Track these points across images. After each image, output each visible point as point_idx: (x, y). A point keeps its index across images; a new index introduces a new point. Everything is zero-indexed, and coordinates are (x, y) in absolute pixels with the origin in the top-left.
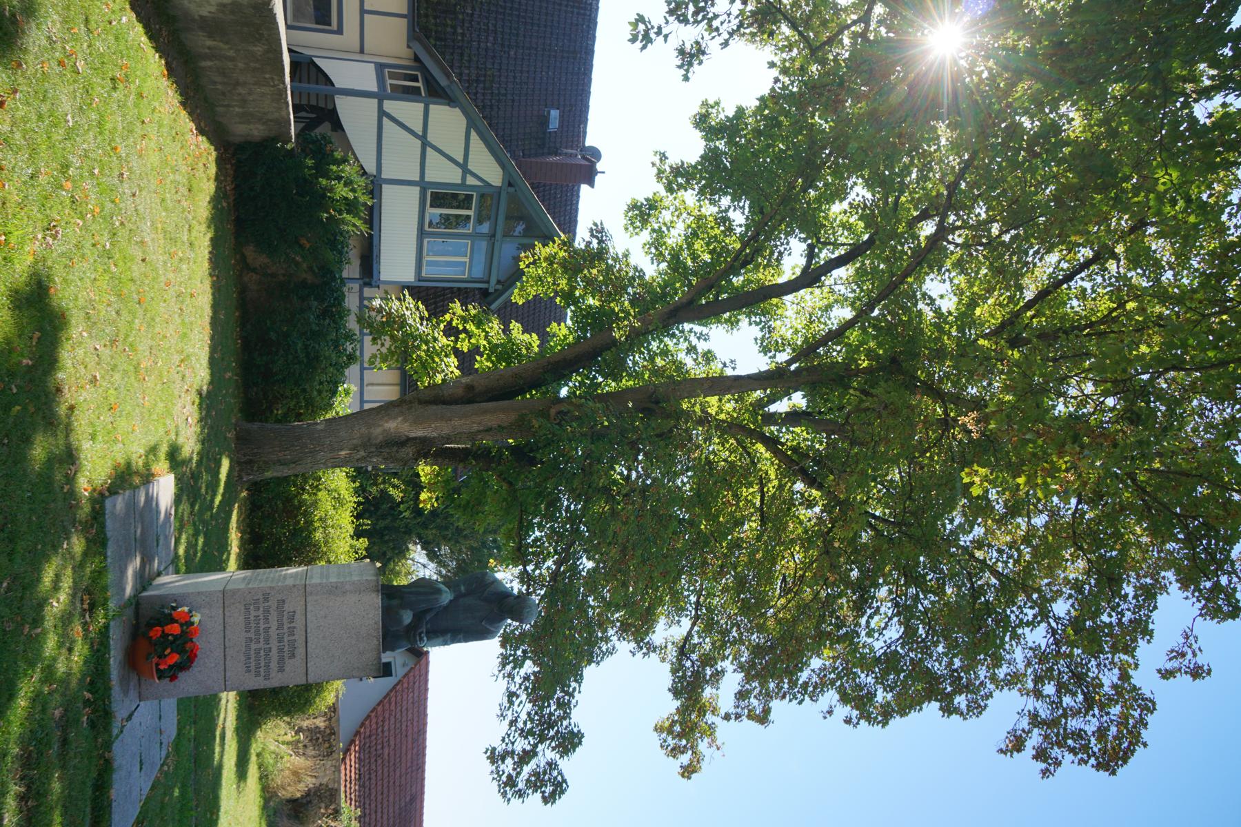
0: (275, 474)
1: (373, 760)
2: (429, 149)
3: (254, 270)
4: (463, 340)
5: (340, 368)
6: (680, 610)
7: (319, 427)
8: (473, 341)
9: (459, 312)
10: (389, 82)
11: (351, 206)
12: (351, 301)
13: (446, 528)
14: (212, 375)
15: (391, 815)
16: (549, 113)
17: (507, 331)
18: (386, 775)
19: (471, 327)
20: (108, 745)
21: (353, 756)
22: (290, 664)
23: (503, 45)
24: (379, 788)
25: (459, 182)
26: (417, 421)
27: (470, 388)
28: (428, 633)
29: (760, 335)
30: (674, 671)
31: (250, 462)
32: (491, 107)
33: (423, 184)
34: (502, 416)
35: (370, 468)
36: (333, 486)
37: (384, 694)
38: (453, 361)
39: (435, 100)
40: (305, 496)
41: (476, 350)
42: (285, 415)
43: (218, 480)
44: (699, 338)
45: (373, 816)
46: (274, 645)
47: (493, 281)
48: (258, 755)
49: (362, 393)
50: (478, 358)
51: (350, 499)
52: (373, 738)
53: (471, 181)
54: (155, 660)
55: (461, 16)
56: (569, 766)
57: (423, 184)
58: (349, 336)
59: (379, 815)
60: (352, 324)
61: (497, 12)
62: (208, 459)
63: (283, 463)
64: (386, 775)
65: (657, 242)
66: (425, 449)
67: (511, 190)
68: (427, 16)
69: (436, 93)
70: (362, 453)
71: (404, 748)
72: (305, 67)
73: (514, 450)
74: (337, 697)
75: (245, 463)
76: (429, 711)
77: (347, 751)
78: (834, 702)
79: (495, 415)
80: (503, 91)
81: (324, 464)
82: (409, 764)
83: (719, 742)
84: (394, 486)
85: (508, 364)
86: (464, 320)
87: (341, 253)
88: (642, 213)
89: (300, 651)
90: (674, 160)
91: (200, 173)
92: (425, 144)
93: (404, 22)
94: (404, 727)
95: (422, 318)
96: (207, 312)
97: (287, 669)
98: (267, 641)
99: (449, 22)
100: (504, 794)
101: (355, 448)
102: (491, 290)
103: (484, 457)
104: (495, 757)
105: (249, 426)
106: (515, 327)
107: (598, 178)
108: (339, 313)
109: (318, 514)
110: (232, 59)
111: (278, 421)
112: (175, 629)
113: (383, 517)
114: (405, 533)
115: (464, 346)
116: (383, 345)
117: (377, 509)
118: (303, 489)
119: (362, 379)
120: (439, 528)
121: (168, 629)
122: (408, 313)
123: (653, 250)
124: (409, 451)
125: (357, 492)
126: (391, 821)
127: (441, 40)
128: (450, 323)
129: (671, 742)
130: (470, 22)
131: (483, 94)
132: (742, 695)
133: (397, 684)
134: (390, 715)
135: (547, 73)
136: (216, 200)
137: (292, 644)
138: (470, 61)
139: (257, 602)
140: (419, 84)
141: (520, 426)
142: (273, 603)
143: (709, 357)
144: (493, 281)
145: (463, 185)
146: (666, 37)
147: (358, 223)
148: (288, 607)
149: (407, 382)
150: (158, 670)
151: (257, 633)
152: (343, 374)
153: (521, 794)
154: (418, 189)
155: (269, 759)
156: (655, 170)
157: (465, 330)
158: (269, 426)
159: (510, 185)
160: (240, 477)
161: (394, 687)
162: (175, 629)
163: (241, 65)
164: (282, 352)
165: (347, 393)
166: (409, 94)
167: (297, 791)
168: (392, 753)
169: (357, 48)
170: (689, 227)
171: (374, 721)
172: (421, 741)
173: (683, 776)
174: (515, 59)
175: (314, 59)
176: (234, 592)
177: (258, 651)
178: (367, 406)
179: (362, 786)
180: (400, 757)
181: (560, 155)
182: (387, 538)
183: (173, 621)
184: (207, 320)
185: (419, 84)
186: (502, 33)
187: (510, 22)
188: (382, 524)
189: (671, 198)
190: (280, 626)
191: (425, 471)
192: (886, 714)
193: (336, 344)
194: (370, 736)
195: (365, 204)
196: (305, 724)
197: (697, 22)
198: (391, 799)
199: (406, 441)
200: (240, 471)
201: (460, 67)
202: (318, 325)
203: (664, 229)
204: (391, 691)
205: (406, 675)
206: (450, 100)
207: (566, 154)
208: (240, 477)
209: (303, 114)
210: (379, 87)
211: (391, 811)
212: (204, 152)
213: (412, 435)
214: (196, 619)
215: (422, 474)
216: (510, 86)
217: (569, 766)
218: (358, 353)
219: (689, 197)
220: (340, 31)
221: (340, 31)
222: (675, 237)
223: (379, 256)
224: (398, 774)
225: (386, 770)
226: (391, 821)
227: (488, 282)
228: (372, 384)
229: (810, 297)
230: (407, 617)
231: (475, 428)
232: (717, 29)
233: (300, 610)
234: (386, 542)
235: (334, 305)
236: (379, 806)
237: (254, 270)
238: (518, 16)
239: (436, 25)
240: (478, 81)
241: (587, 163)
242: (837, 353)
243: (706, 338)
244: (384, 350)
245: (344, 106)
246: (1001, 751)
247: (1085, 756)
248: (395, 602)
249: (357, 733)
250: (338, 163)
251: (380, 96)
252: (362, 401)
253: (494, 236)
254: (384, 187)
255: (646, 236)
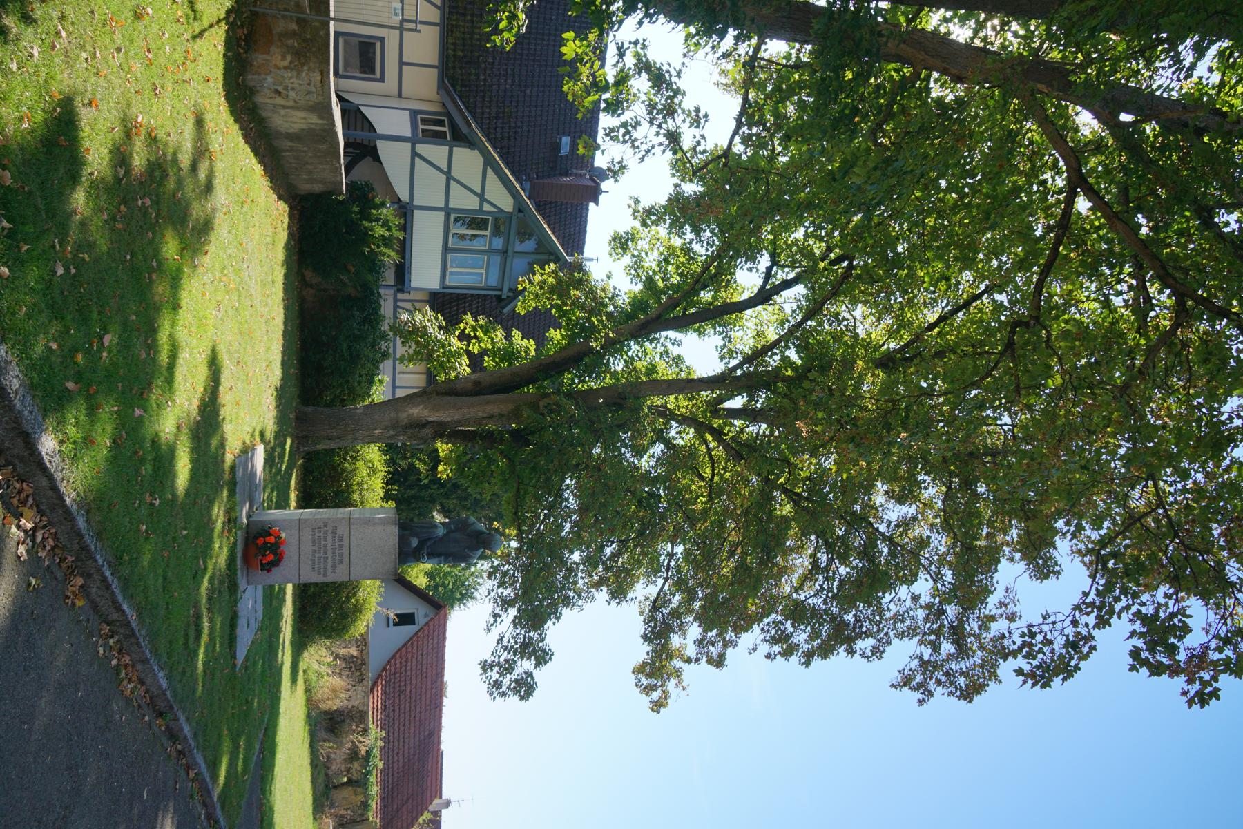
0: (325, 447)
1: (397, 695)
2: (452, 182)
3: (311, 286)
4: (474, 344)
5: (376, 364)
6: (656, 571)
7: (358, 411)
8: (482, 345)
9: (471, 322)
10: (421, 127)
11: (387, 241)
12: (386, 308)
13: (466, 499)
14: (283, 373)
15: (412, 745)
16: (561, 139)
17: (508, 337)
18: (408, 709)
19: (480, 334)
20: (236, 602)
21: (379, 690)
22: (340, 568)
23: (520, 86)
24: (402, 720)
25: (478, 208)
26: (435, 409)
27: (477, 383)
28: (428, 555)
29: (721, 343)
30: (647, 622)
31: (306, 437)
32: (509, 139)
33: (447, 211)
34: (501, 406)
35: (400, 444)
36: (368, 458)
37: (408, 638)
38: (465, 360)
39: (459, 143)
40: (346, 465)
41: (484, 352)
42: (333, 400)
43: (285, 450)
44: (673, 344)
45: (396, 743)
46: (330, 555)
47: (506, 289)
48: (305, 672)
49: (394, 380)
50: (486, 358)
51: (382, 470)
52: (397, 675)
53: (487, 207)
54: (260, 557)
55: (483, 66)
56: (541, 675)
57: (447, 211)
58: (384, 337)
59: (401, 744)
60: (385, 327)
61: (515, 59)
62: (280, 436)
63: (330, 438)
64: (408, 709)
65: (637, 266)
66: (442, 431)
67: (521, 215)
68: (454, 68)
69: (460, 138)
70: (392, 432)
71: (424, 688)
72: (353, 115)
73: (513, 433)
74: (367, 626)
75: (303, 437)
76: (447, 657)
77: (375, 684)
78: (758, 641)
79: (497, 405)
80: (519, 124)
81: (362, 440)
82: (428, 702)
83: (684, 684)
84: (420, 460)
85: (510, 364)
86: (474, 329)
87: (378, 273)
88: (621, 243)
89: (346, 560)
90: (646, 203)
91: (280, 229)
92: (449, 178)
93: (435, 71)
94: (424, 670)
95: (440, 328)
96: (281, 327)
97: (338, 571)
98: (325, 553)
99: (473, 71)
100: (491, 695)
101: (386, 428)
102: (504, 297)
103: (490, 438)
104: (486, 667)
105: (306, 409)
106: (516, 333)
107: (602, 197)
108: (376, 320)
109: (356, 480)
110: (305, 152)
111: (327, 405)
112: (272, 539)
113: (410, 487)
114: (430, 502)
115: (475, 349)
116: (410, 347)
117: (406, 480)
118: (345, 459)
119: (394, 368)
120: (461, 499)
121: (267, 539)
122: (428, 324)
123: (633, 272)
124: (428, 432)
125: (387, 463)
126: (412, 750)
127: (466, 86)
128: (463, 331)
129: (644, 681)
130: (492, 69)
131: (502, 128)
132: (700, 643)
133: (419, 631)
134: (412, 657)
135: (560, 105)
136: (288, 247)
137: (341, 555)
138: (490, 102)
139: (320, 528)
140: (446, 129)
141: (515, 414)
142: (329, 529)
143: (678, 359)
144: (506, 289)
145: (481, 210)
146: (603, 151)
147: (392, 254)
148: (339, 532)
149: (431, 377)
150: (261, 564)
151: (319, 547)
152: (378, 368)
153: (503, 694)
154: (443, 213)
155: (313, 677)
156: (631, 211)
157: (476, 337)
158: (321, 409)
159: (520, 211)
160: (298, 448)
161: (416, 633)
162: (272, 539)
163: (310, 154)
164: (331, 352)
165: (381, 382)
166: (437, 137)
167: (335, 705)
168: (414, 690)
169: (396, 93)
170: (662, 254)
171: (398, 660)
172: (439, 683)
173: (652, 710)
174: (531, 96)
175: (361, 108)
176: (306, 520)
177: (319, 558)
178: (400, 393)
179: (387, 716)
180: (420, 695)
181: (571, 175)
182: (414, 505)
183: (270, 535)
184: (281, 333)
185: (446, 129)
186: (519, 76)
187: (527, 66)
188: (410, 493)
189: (646, 231)
190: (334, 543)
191: (443, 448)
192: (808, 657)
193: (373, 345)
194: (395, 674)
195: (398, 239)
196: (342, 652)
197: (625, 142)
198: (412, 731)
199: (426, 424)
200: (299, 443)
201: (482, 107)
202: (359, 330)
203: (643, 254)
204: (414, 636)
205: (427, 623)
206: (470, 143)
207: (576, 175)
208: (298, 448)
209: (350, 150)
210: (412, 133)
211: (412, 741)
212: (283, 208)
213: (431, 419)
214: (283, 535)
215: (440, 450)
216: (526, 119)
217: (541, 675)
218: (391, 351)
219: (662, 231)
220: (382, 80)
221: (382, 80)
222: (651, 261)
223: (410, 268)
224: (418, 710)
225: (408, 705)
226: (412, 750)
227: (501, 290)
228: (403, 373)
229: (763, 313)
230: (415, 542)
231: (480, 415)
232: (638, 147)
233: (346, 534)
234: (414, 509)
235: (372, 314)
236: (401, 736)
237: (311, 286)
238: (534, 60)
239: (462, 74)
240: (497, 118)
241: (593, 184)
242: (774, 361)
243: (676, 343)
244: (411, 351)
245: (383, 148)
246: (893, 686)
247: (954, 690)
248: (407, 532)
249: (384, 669)
250: (377, 207)
251: (413, 140)
252: (394, 387)
253: (506, 252)
254: (416, 212)
255: (627, 260)
